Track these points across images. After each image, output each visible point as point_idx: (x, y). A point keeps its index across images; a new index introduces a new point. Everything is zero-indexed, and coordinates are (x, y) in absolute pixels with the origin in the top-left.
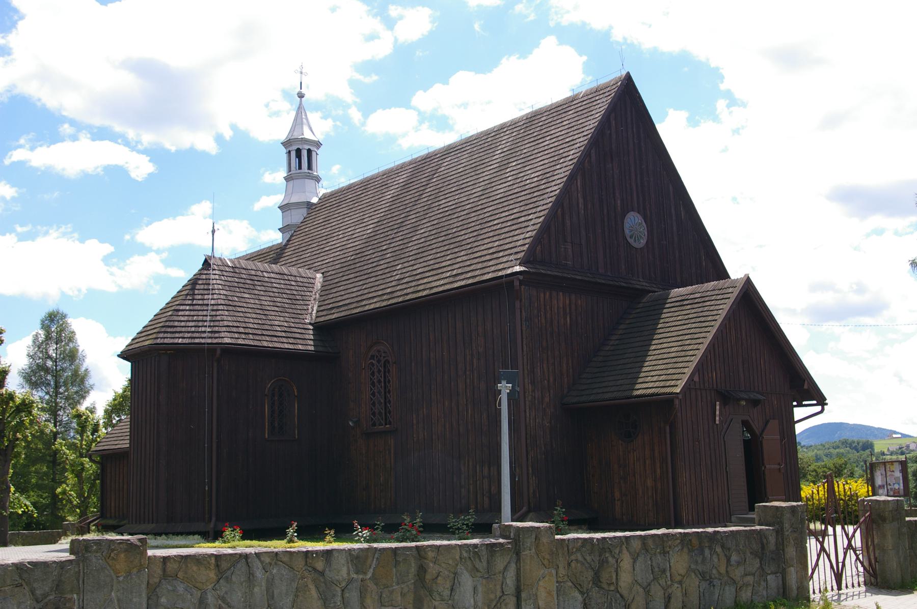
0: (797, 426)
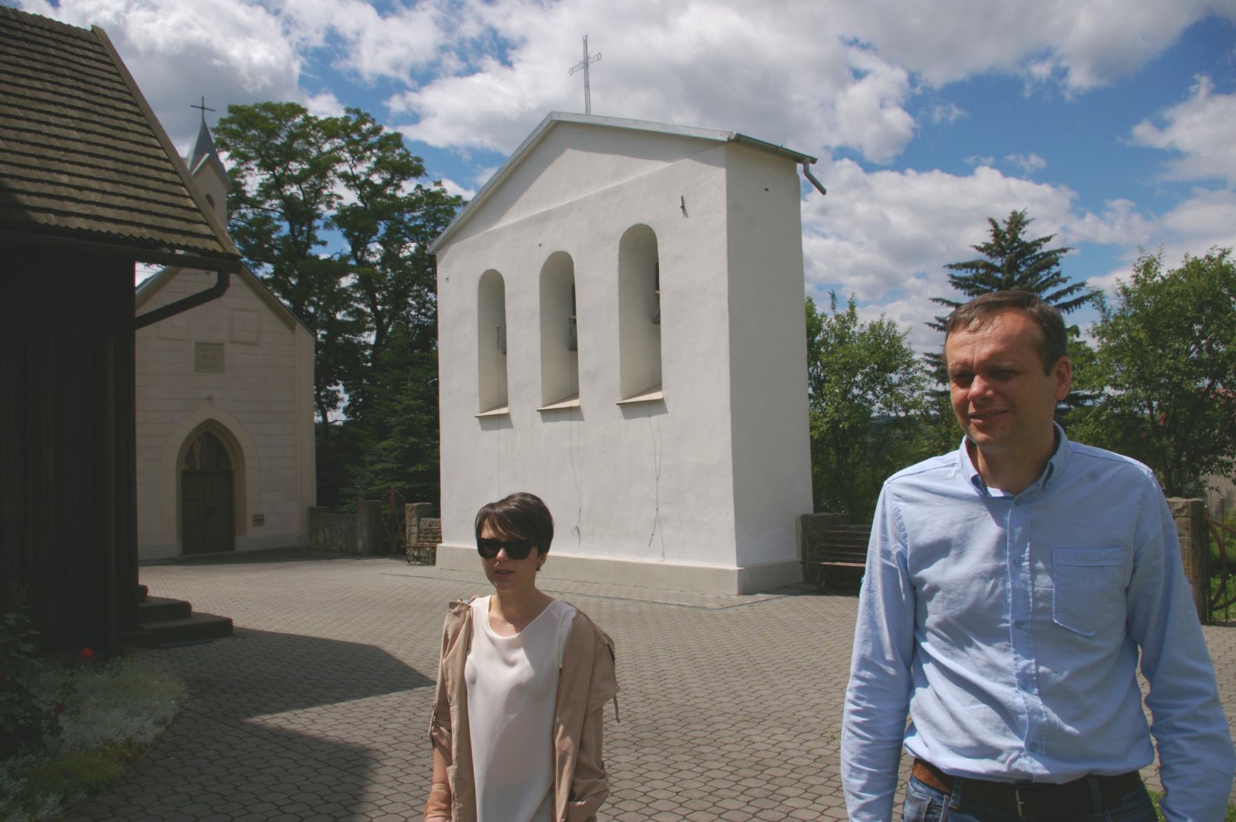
0: (144, 336)
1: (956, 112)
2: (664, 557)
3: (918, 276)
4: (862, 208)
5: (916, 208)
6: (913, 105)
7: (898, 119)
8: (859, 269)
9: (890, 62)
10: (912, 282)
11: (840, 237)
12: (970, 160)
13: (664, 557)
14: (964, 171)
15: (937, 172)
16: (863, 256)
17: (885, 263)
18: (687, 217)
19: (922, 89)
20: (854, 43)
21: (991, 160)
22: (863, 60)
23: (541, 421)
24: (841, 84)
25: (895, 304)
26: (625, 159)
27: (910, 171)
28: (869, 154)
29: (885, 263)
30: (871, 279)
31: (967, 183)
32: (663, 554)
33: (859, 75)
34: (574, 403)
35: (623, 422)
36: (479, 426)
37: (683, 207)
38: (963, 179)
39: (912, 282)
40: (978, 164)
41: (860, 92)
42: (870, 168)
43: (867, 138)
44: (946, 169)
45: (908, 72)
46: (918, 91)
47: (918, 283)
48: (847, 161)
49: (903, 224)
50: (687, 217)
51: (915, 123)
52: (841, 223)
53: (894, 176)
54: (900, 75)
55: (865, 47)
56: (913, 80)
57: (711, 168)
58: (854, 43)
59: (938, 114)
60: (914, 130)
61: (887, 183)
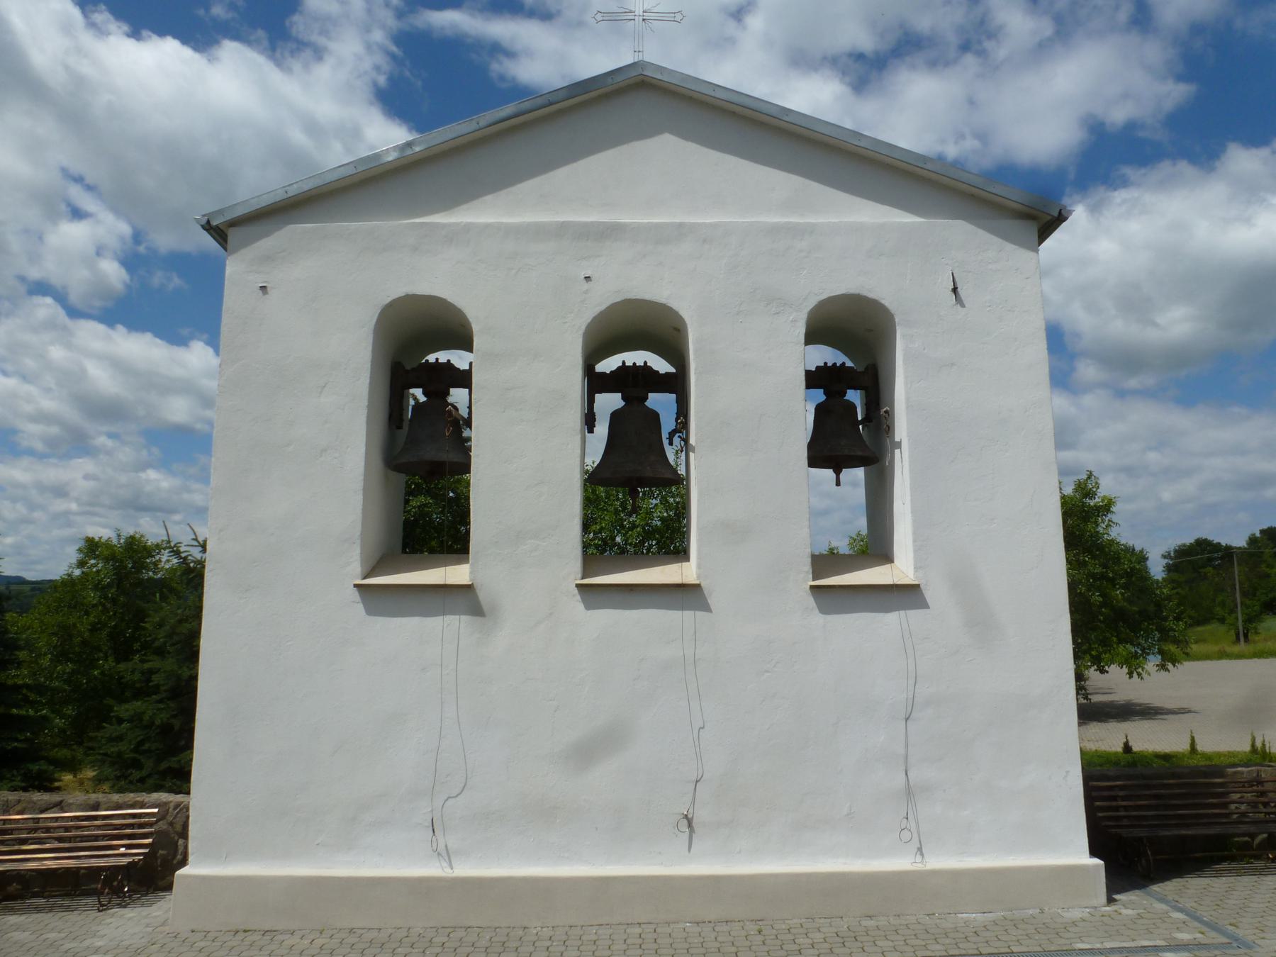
1: (176, 281)
2: (922, 854)
3: (110, 435)
4: (57, 353)
5: (120, 366)
6: (131, 261)
7: (112, 271)
8: (42, 417)
9: (117, 211)
10: (102, 440)
11: (25, 378)
12: (185, 332)
13: (922, 854)
14: (178, 340)
15: (148, 336)
16: (48, 405)
17: (72, 415)
18: (963, 305)
19: (148, 248)
20: (79, 180)
21: (205, 336)
22: (87, 202)
23: (581, 606)
24: (52, 215)
25: (80, 460)
26: (814, 186)
27: (120, 328)
28: (74, 298)
29: (72, 415)
30: (54, 430)
31: (179, 353)
32: (920, 849)
33: (77, 214)
34: (456, 574)
35: (818, 619)
36: (360, 607)
37: (955, 290)
38: (175, 348)
39: (102, 440)
40: (192, 337)
41: (73, 234)
42: (74, 313)
43: (77, 281)
44: (158, 335)
45: (134, 227)
46: (142, 249)
47: (109, 443)
48: (49, 300)
49: (102, 379)
50: (963, 305)
51: (131, 280)
52: (30, 363)
53: (101, 328)
54: (125, 229)
55: (90, 188)
56: (137, 237)
57: (1010, 247)
58: (79, 180)
59: (157, 279)
60: (128, 286)
61: (91, 333)
